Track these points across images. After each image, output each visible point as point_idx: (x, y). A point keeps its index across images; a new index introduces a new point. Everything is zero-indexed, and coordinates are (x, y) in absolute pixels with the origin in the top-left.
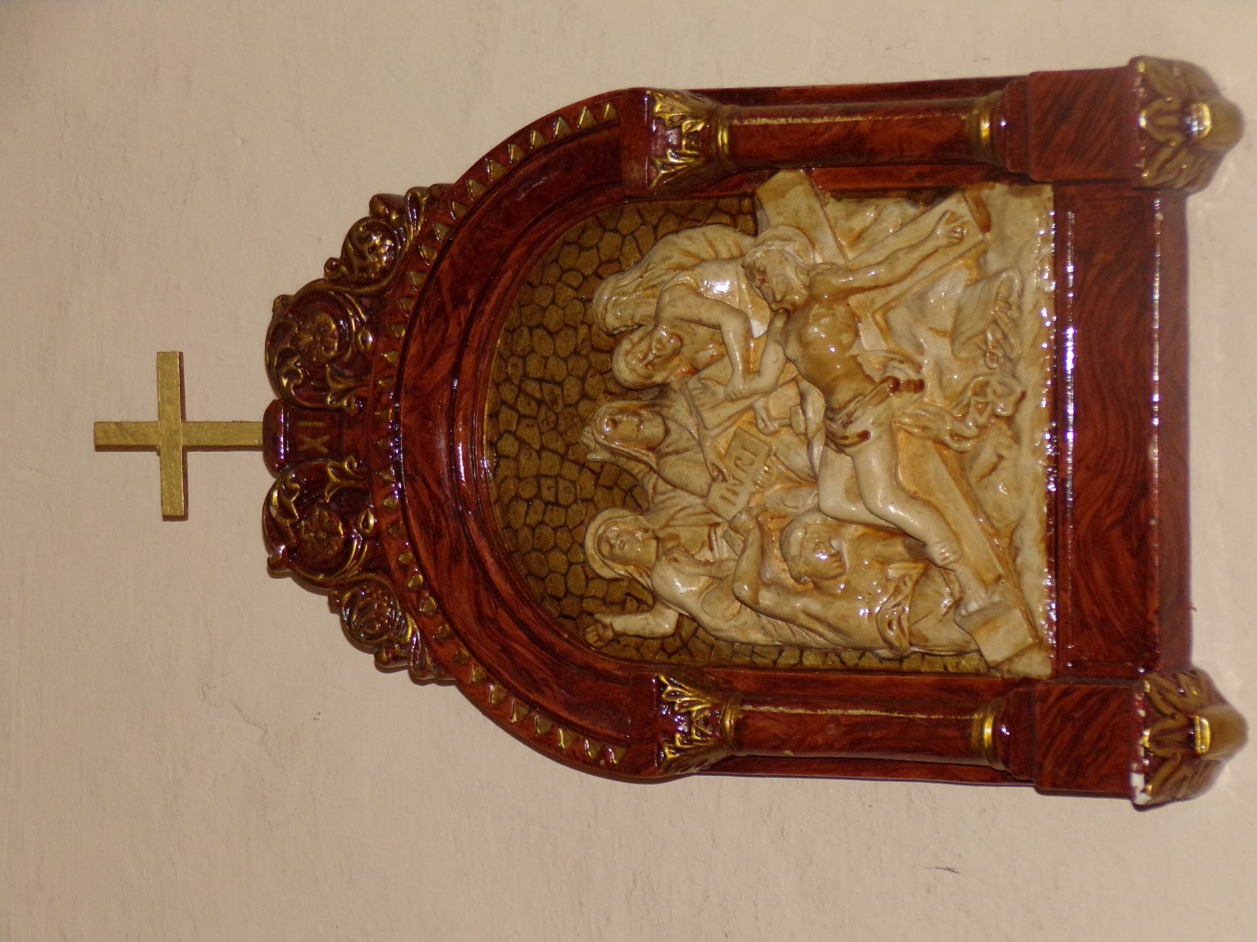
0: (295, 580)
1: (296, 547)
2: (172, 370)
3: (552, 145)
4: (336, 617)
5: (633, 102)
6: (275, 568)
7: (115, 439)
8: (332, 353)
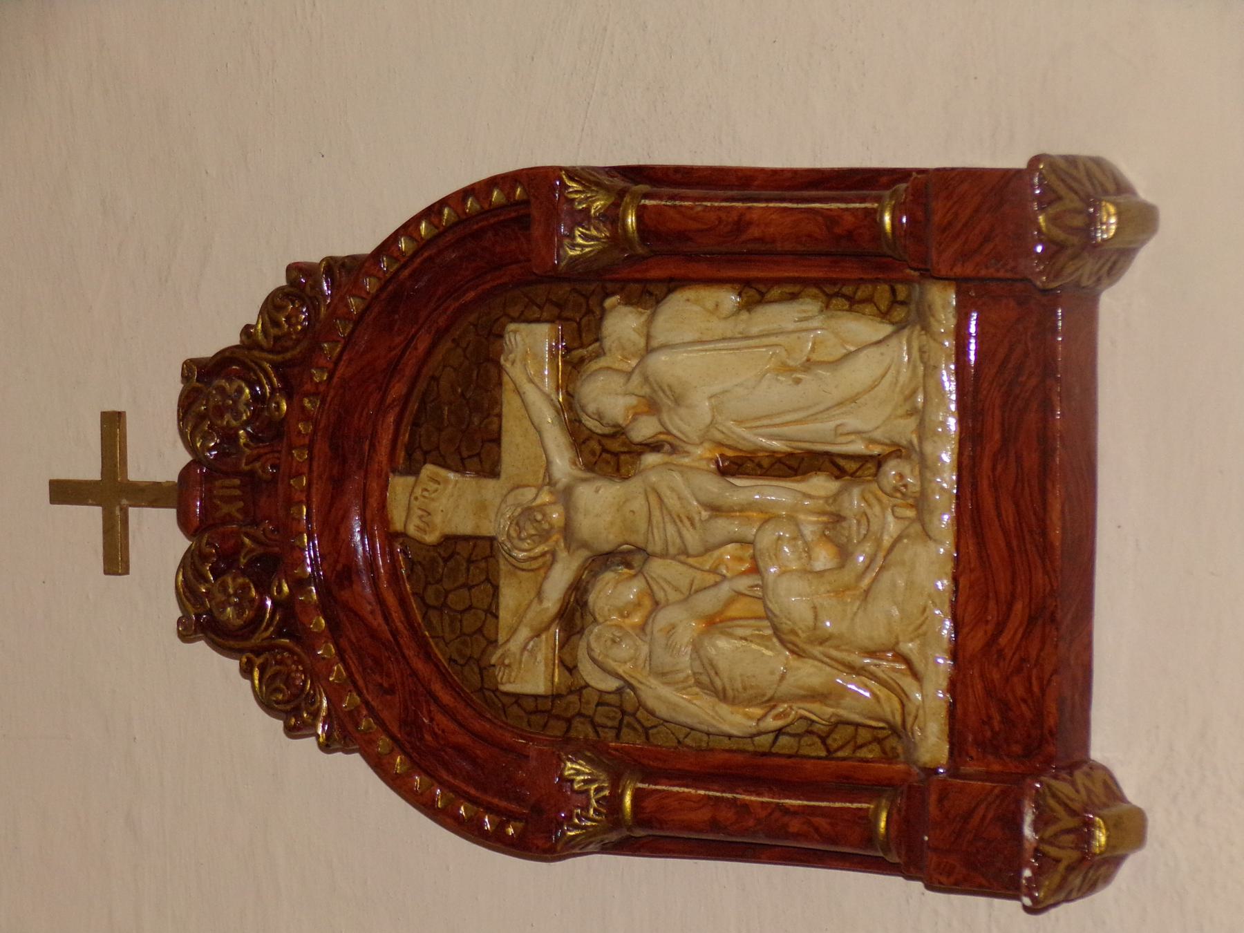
4: (247, 683)
6: (187, 632)
7: (63, 492)
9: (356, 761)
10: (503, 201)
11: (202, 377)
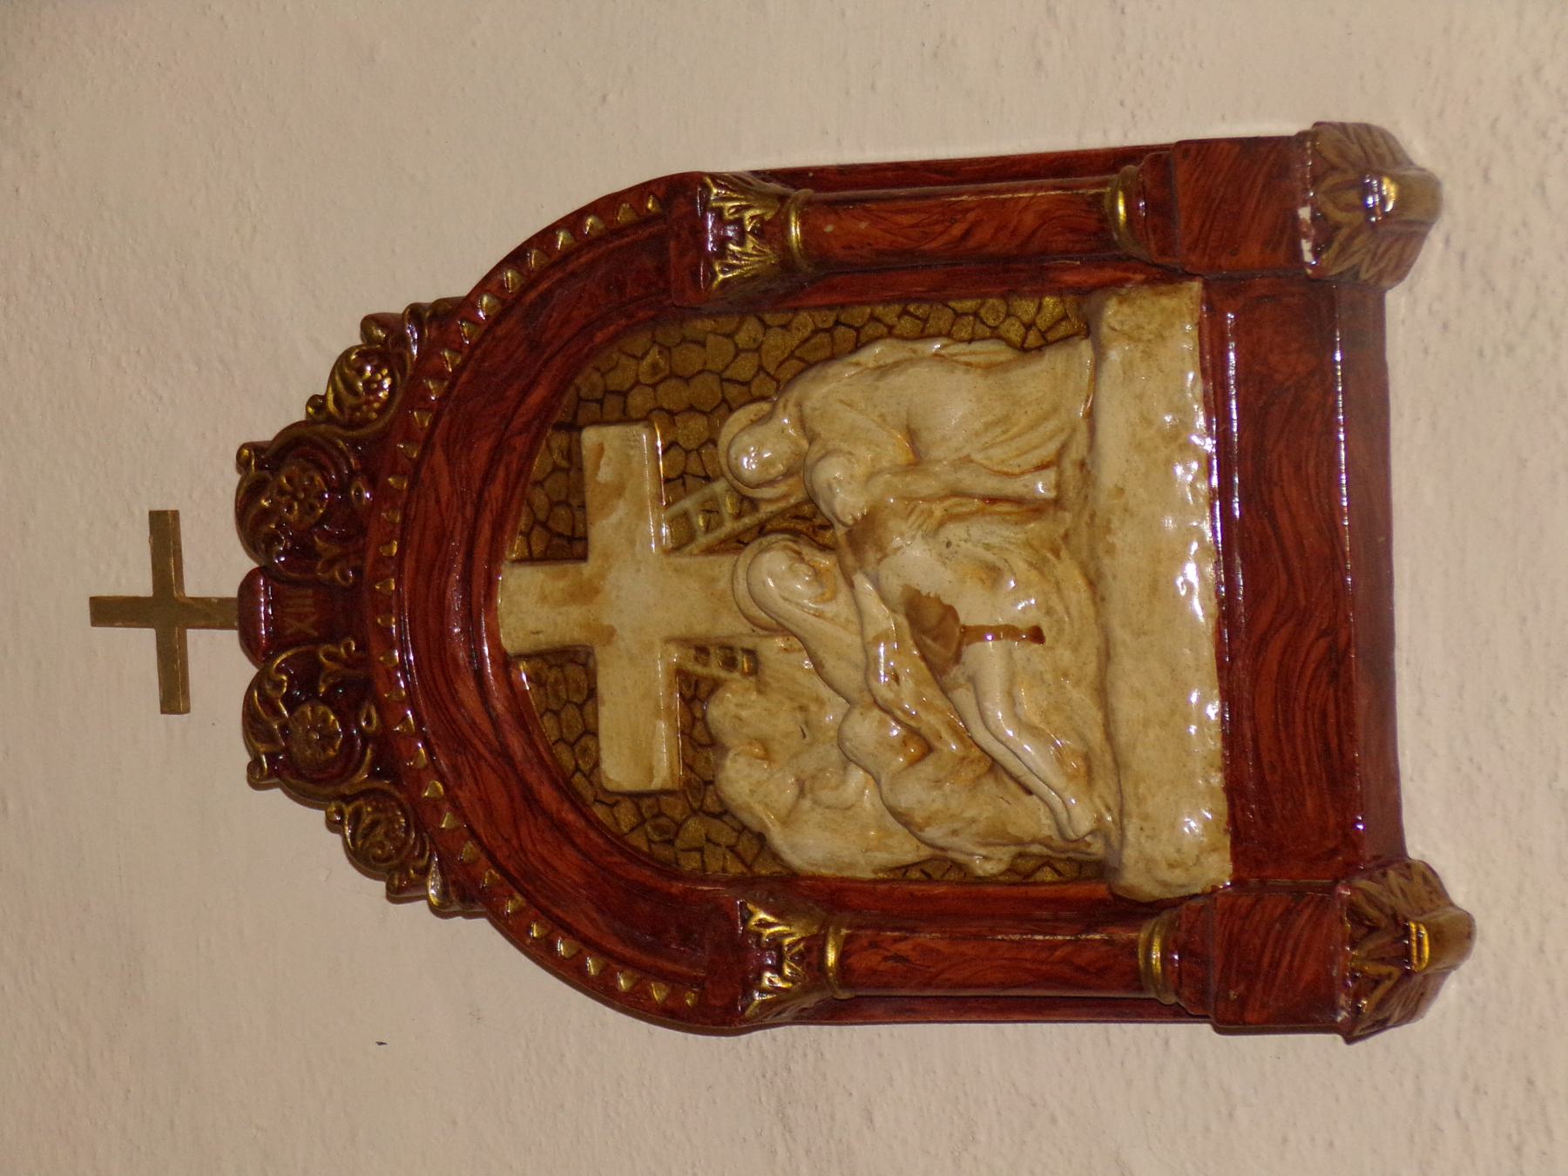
1: (280, 760)
3: (583, 243)
4: (337, 838)
5: (680, 191)
6: (258, 777)
7: (107, 611)
8: (331, 753)
9: (481, 928)
10: (546, 261)
11: (265, 467)
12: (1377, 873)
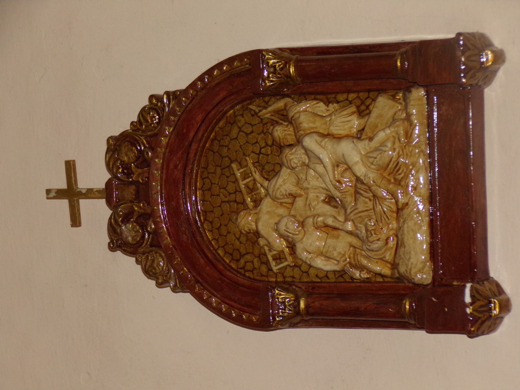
0: (122, 252)
1: (117, 243)
2: (70, 167)
5: (255, 57)
9: (188, 296)
11: (116, 145)
12: (481, 283)
